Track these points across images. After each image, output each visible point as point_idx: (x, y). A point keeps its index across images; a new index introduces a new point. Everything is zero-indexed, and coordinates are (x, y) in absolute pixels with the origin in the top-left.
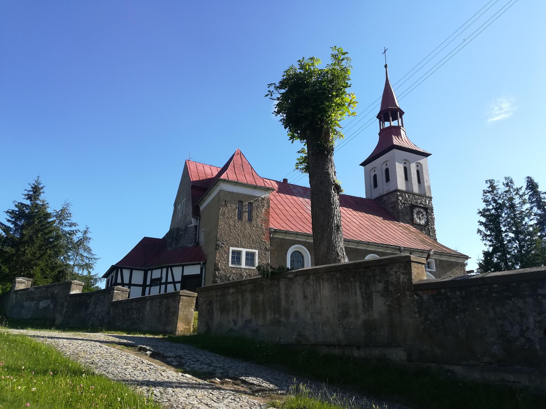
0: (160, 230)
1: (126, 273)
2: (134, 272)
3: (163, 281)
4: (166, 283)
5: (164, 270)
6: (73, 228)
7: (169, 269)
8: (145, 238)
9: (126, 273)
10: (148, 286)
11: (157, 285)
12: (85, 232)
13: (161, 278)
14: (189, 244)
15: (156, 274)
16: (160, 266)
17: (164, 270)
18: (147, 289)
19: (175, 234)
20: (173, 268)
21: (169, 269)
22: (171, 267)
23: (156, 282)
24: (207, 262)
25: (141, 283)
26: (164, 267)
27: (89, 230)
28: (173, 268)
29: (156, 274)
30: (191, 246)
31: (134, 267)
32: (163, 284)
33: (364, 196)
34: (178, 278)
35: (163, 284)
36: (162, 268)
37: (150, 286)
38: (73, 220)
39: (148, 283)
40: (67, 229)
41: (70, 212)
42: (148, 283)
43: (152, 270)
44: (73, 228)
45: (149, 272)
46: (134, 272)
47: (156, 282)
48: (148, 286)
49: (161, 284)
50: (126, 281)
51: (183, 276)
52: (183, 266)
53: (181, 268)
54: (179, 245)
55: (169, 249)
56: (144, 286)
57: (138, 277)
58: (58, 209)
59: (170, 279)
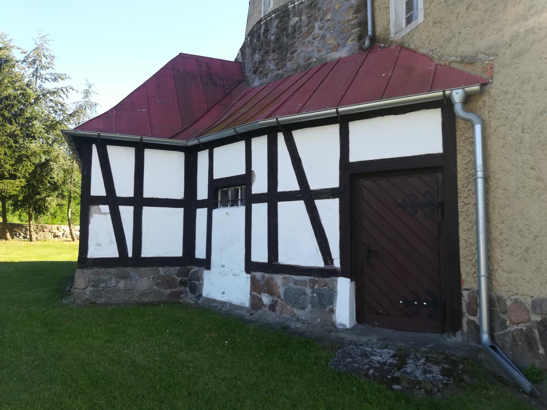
0: (223, 40)
1: (121, 159)
2: (151, 156)
3: (260, 186)
4: (273, 197)
5: (260, 145)
6: (60, 84)
7: (281, 138)
8: (182, 58)
9: (121, 159)
10: (202, 204)
11: (234, 203)
12: (87, 93)
13: (247, 178)
14: (336, 48)
15: (228, 161)
16: (241, 129)
17: (260, 145)
18: (201, 214)
19: (273, 30)
20: (298, 135)
21: (281, 138)
22: (288, 129)
23: (232, 191)
24: (494, 90)
25: (179, 194)
26: (258, 133)
27: (93, 89)
28: (298, 135)
29: (228, 161)
30: (343, 53)
31: (146, 139)
32: (259, 198)
33: (120, 206)
34: (324, 173)
35: (259, 198)
36: (247, 137)
37: (211, 204)
38: (58, 69)
39: (202, 193)
40: (49, 86)
41: (53, 53)
42: (202, 193)
43: (211, 146)
44: (60, 84)
45: (203, 157)
46: (151, 156)
47: (232, 191)
48: (202, 204)
49: (250, 200)
50: (124, 187)
51: (344, 163)
52: (343, 121)
53: (333, 132)
54: (289, 65)
55: (257, 83)
56: (189, 203)
57: (165, 173)
58: (29, 47)
59: (287, 181)
